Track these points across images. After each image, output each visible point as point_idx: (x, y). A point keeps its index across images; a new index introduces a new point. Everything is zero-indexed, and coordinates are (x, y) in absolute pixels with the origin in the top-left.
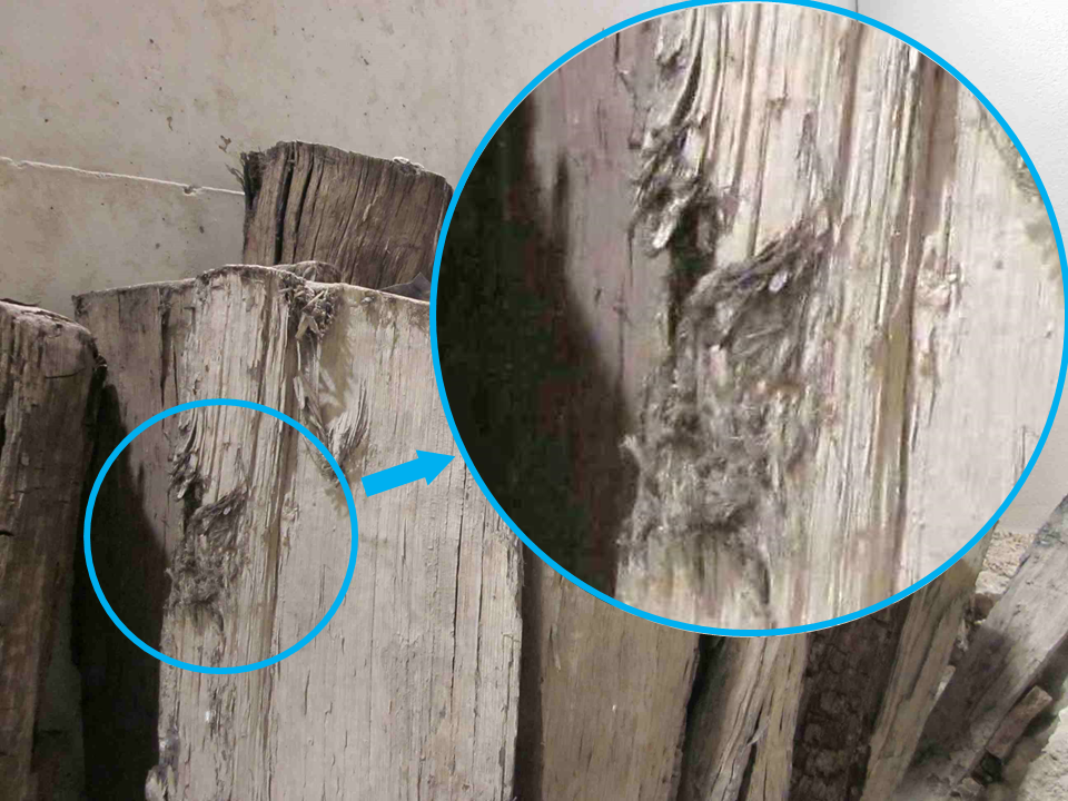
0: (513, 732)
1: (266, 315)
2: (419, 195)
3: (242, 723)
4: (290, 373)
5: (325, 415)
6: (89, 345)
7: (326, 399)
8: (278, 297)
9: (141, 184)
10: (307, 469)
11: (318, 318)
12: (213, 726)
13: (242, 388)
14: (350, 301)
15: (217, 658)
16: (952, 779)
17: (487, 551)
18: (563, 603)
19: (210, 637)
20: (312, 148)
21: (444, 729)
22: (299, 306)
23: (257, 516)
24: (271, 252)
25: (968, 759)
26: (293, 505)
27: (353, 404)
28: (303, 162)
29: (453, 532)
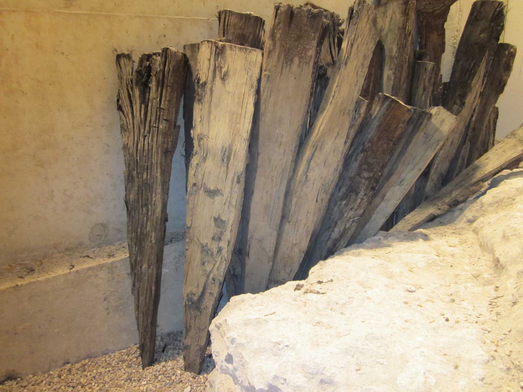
0: (250, 128)
1: (211, 49)
2: (252, 21)
3: (205, 121)
4: (215, 61)
5: (221, 68)
6: (185, 56)
7: (222, 65)
8: (213, 46)
9: (198, 19)
10: (218, 78)
11: (220, 50)
12: (201, 121)
13: (206, 63)
14: (227, 46)
15: (201, 109)
16: (440, 205)
17: (249, 95)
18: (265, 108)
19: (200, 106)
20: (230, 11)
21: (238, 126)
22: (217, 47)
23: (209, 86)
24: (222, 35)
25: (447, 200)
26: (215, 84)
27: (226, 67)
28: (228, 14)
29: (243, 91)
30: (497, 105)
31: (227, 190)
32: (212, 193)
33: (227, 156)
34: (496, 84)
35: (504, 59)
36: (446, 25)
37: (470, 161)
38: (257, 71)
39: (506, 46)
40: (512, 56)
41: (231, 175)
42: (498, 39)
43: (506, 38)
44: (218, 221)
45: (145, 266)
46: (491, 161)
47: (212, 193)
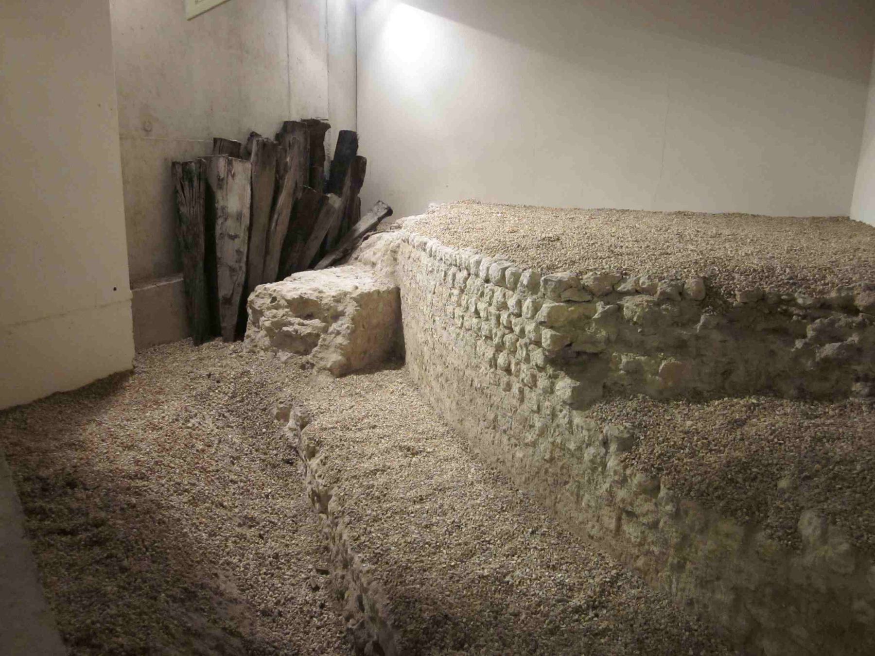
31: (242, 235)
32: (233, 237)
33: (239, 217)
37: (349, 228)
39: (360, 158)
40: (365, 163)
41: (243, 227)
44: (238, 252)
46: (362, 225)
47: (233, 237)
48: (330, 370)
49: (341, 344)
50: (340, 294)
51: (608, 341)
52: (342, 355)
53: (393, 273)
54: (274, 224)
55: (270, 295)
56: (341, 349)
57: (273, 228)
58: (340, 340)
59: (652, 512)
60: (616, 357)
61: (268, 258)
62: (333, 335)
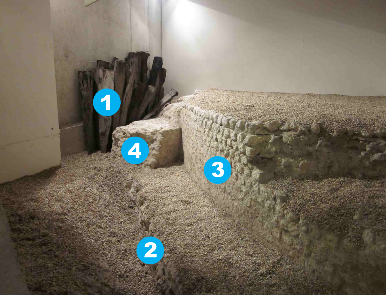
30: (163, 86)
34: (163, 80)
35: (327, 227)
36: (147, 63)
37: (158, 101)
38: (113, 76)
39: (164, 69)
42: (161, 67)
43: (163, 67)
45: (90, 125)
46: (164, 100)
48: (150, 165)
49: (155, 154)
50: (155, 131)
51: (276, 152)
52: (155, 159)
53: (178, 121)
54: (124, 99)
55: (123, 131)
56: (155, 156)
57: (124, 101)
58: (154, 152)
59: (296, 230)
60: (279, 160)
61: (122, 115)
62: (151, 150)
